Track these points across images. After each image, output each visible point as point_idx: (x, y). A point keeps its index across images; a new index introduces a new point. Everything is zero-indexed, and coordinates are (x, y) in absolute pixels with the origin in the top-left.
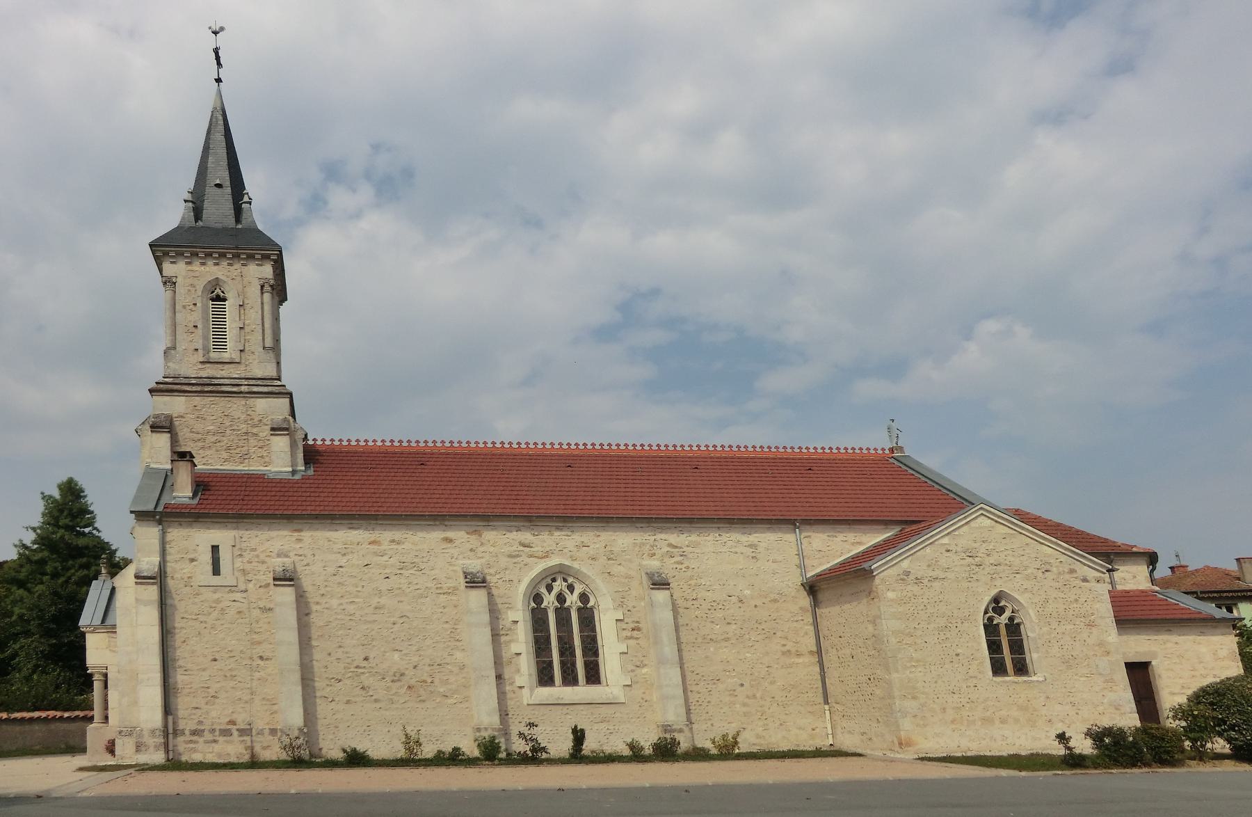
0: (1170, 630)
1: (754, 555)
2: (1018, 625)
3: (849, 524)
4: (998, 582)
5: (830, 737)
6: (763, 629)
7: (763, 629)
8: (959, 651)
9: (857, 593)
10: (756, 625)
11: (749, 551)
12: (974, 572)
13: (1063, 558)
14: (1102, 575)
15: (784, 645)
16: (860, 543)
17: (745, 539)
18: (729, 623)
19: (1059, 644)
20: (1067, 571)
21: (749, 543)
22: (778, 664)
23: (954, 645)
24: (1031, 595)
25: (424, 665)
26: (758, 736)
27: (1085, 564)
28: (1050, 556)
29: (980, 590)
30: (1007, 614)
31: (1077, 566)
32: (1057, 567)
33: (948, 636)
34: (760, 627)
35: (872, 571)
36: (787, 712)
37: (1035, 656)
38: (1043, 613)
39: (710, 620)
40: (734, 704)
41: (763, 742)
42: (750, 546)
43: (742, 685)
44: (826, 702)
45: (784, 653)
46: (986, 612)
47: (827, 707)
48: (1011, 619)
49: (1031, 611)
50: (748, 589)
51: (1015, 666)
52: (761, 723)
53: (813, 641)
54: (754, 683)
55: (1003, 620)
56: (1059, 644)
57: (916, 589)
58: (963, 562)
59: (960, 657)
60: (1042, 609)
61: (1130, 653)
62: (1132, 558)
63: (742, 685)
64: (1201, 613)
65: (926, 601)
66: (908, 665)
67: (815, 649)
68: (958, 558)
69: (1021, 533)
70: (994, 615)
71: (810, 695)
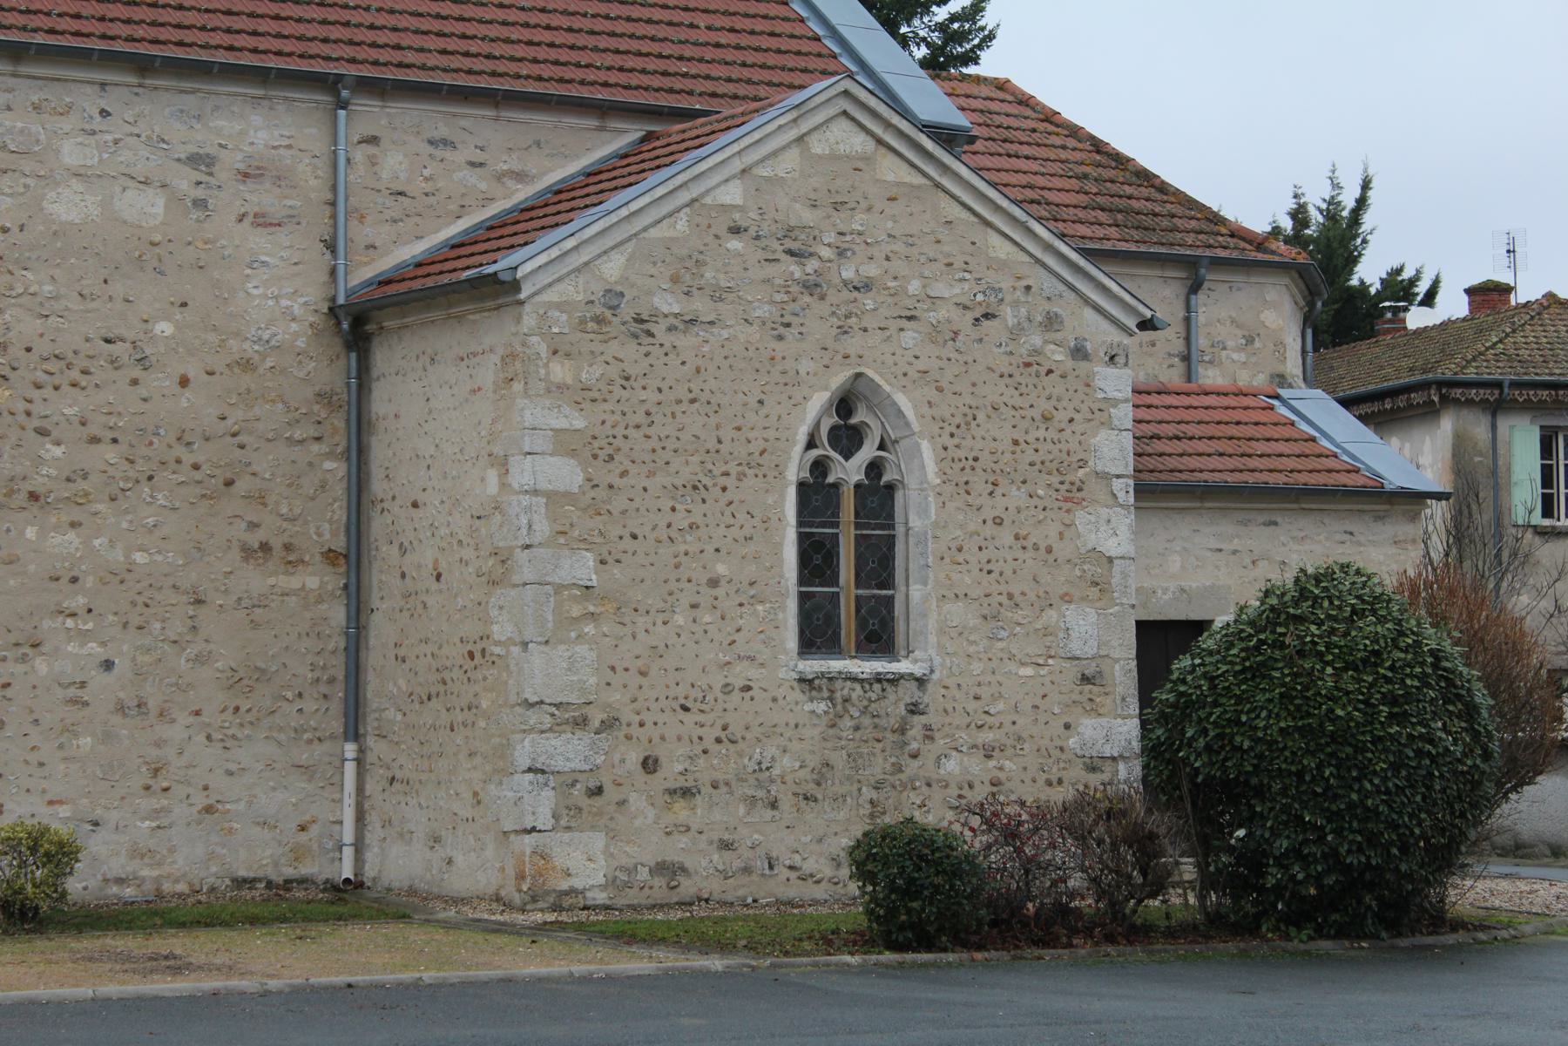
0: (1275, 524)
1: (200, 193)
2: (891, 488)
3: (497, 106)
4: (853, 344)
5: (348, 852)
6: (196, 467)
7: (196, 467)
8: (721, 569)
9: (475, 355)
10: (180, 451)
11: (184, 180)
12: (796, 307)
13: (1038, 278)
14: (1126, 340)
15: (253, 526)
16: (520, 177)
17: (186, 135)
18: (95, 440)
19: (984, 556)
20: (1039, 319)
21: (192, 149)
22: (226, 592)
23: (710, 549)
24: (932, 394)
25: (625, 552)
26: (136, 853)
27: (1087, 301)
28: (1002, 265)
29: (805, 366)
30: (867, 452)
31: (1066, 306)
32: (1016, 304)
33: (697, 518)
34: (188, 459)
35: (515, 286)
36: (233, 767)
37: (916, 592)
38: (961, 454)
39: (37, 423)
40: (76, 735)
41: (145, 873)
42: (194, 160)
43: (108, 665)
44: (354, 732)
45: (247, 553)
46: (811, 445)
47: (350, 749)
48: (875, 468)
49: (925, 446)
50: (168, 318)
51: (862, 623)
52: (147, 803)
53: (340, 513)
54: (147, 659)
55: (849, 471)
56: (984, 556)
57: (630, 351)
58: (770, 270)
59: (720, 592)
60: (956, 441)
61: (1165, 590)
62: (1253, 279)
63: (108, 665)
64: (1357, 471)
65: (651, 396)
66: (576, 611)
67: (340, 544)
68: (761, 255)
69: (938, 185)
70: (833, 454)
71: (309, 705)
